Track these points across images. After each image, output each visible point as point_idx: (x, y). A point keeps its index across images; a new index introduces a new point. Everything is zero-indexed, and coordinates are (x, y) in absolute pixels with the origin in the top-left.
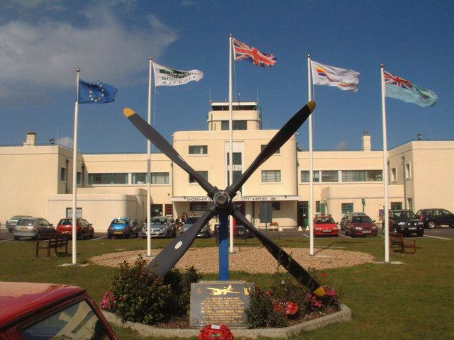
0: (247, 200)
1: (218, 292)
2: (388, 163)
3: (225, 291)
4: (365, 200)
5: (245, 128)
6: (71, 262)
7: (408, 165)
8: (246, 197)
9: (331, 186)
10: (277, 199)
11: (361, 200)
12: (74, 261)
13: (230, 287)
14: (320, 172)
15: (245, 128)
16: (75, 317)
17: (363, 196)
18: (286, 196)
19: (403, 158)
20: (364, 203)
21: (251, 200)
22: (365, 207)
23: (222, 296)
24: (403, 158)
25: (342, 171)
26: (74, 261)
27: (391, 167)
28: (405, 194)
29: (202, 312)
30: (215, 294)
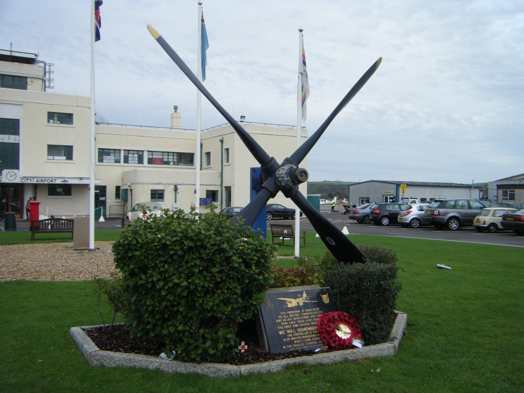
0: (29, 182)
1: (292, 303)
2: (201, 146)
3: (301, 301)
4: (178, 187)
5: (24, 87)
6: (293, 254)
7: (227, 150)
8: (24, 178)
9: (137, 169)
10: (71, 182)
11: (173, 187)
12: (297, 253)
13: (305, 295)
14: (122, 153)
15: (24, 87)
16: (367, 348)
17: (175, 182)
18: (81, 179)
19: (222, 141)
20: (176, 189)
21: (35, 181)
22: (177, 195)
23: (298, 307)
24: (222, 141)
25: (124, 150)
26: (297, 253)
27: (205, 151)
28: (222, 182)
29: (281, 333)
30: (290, 305)
